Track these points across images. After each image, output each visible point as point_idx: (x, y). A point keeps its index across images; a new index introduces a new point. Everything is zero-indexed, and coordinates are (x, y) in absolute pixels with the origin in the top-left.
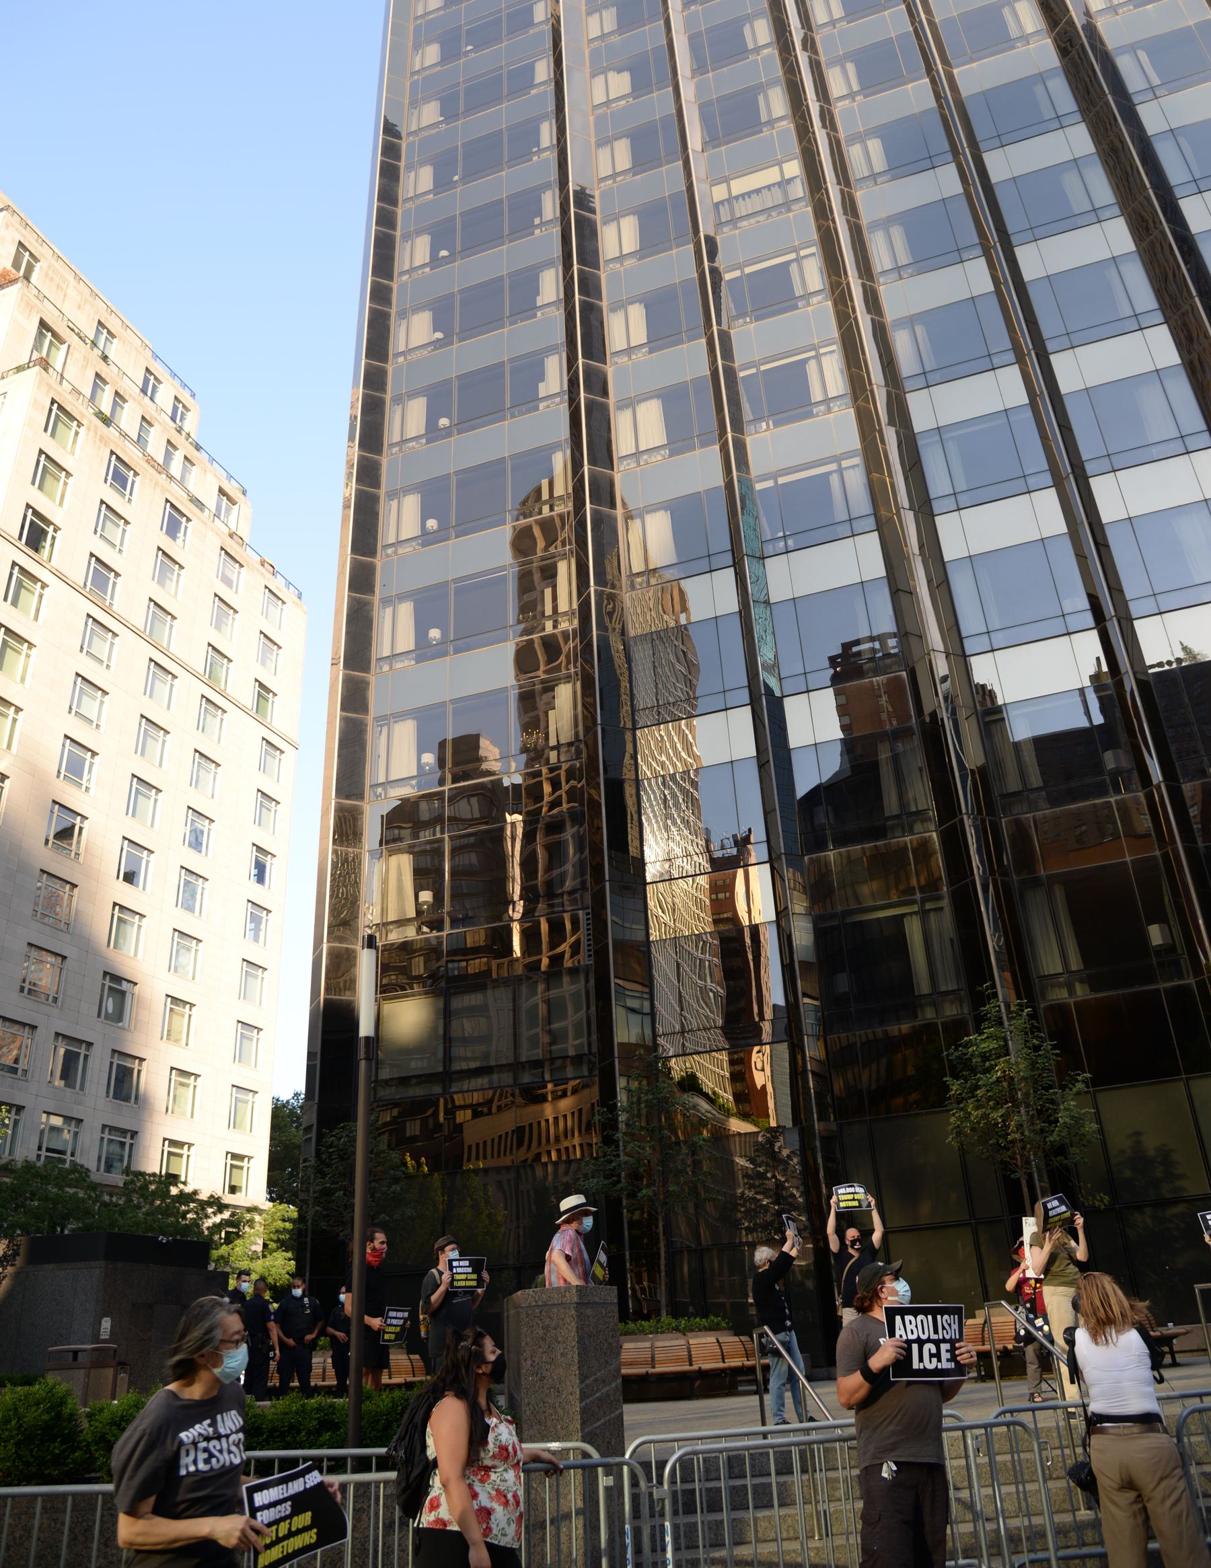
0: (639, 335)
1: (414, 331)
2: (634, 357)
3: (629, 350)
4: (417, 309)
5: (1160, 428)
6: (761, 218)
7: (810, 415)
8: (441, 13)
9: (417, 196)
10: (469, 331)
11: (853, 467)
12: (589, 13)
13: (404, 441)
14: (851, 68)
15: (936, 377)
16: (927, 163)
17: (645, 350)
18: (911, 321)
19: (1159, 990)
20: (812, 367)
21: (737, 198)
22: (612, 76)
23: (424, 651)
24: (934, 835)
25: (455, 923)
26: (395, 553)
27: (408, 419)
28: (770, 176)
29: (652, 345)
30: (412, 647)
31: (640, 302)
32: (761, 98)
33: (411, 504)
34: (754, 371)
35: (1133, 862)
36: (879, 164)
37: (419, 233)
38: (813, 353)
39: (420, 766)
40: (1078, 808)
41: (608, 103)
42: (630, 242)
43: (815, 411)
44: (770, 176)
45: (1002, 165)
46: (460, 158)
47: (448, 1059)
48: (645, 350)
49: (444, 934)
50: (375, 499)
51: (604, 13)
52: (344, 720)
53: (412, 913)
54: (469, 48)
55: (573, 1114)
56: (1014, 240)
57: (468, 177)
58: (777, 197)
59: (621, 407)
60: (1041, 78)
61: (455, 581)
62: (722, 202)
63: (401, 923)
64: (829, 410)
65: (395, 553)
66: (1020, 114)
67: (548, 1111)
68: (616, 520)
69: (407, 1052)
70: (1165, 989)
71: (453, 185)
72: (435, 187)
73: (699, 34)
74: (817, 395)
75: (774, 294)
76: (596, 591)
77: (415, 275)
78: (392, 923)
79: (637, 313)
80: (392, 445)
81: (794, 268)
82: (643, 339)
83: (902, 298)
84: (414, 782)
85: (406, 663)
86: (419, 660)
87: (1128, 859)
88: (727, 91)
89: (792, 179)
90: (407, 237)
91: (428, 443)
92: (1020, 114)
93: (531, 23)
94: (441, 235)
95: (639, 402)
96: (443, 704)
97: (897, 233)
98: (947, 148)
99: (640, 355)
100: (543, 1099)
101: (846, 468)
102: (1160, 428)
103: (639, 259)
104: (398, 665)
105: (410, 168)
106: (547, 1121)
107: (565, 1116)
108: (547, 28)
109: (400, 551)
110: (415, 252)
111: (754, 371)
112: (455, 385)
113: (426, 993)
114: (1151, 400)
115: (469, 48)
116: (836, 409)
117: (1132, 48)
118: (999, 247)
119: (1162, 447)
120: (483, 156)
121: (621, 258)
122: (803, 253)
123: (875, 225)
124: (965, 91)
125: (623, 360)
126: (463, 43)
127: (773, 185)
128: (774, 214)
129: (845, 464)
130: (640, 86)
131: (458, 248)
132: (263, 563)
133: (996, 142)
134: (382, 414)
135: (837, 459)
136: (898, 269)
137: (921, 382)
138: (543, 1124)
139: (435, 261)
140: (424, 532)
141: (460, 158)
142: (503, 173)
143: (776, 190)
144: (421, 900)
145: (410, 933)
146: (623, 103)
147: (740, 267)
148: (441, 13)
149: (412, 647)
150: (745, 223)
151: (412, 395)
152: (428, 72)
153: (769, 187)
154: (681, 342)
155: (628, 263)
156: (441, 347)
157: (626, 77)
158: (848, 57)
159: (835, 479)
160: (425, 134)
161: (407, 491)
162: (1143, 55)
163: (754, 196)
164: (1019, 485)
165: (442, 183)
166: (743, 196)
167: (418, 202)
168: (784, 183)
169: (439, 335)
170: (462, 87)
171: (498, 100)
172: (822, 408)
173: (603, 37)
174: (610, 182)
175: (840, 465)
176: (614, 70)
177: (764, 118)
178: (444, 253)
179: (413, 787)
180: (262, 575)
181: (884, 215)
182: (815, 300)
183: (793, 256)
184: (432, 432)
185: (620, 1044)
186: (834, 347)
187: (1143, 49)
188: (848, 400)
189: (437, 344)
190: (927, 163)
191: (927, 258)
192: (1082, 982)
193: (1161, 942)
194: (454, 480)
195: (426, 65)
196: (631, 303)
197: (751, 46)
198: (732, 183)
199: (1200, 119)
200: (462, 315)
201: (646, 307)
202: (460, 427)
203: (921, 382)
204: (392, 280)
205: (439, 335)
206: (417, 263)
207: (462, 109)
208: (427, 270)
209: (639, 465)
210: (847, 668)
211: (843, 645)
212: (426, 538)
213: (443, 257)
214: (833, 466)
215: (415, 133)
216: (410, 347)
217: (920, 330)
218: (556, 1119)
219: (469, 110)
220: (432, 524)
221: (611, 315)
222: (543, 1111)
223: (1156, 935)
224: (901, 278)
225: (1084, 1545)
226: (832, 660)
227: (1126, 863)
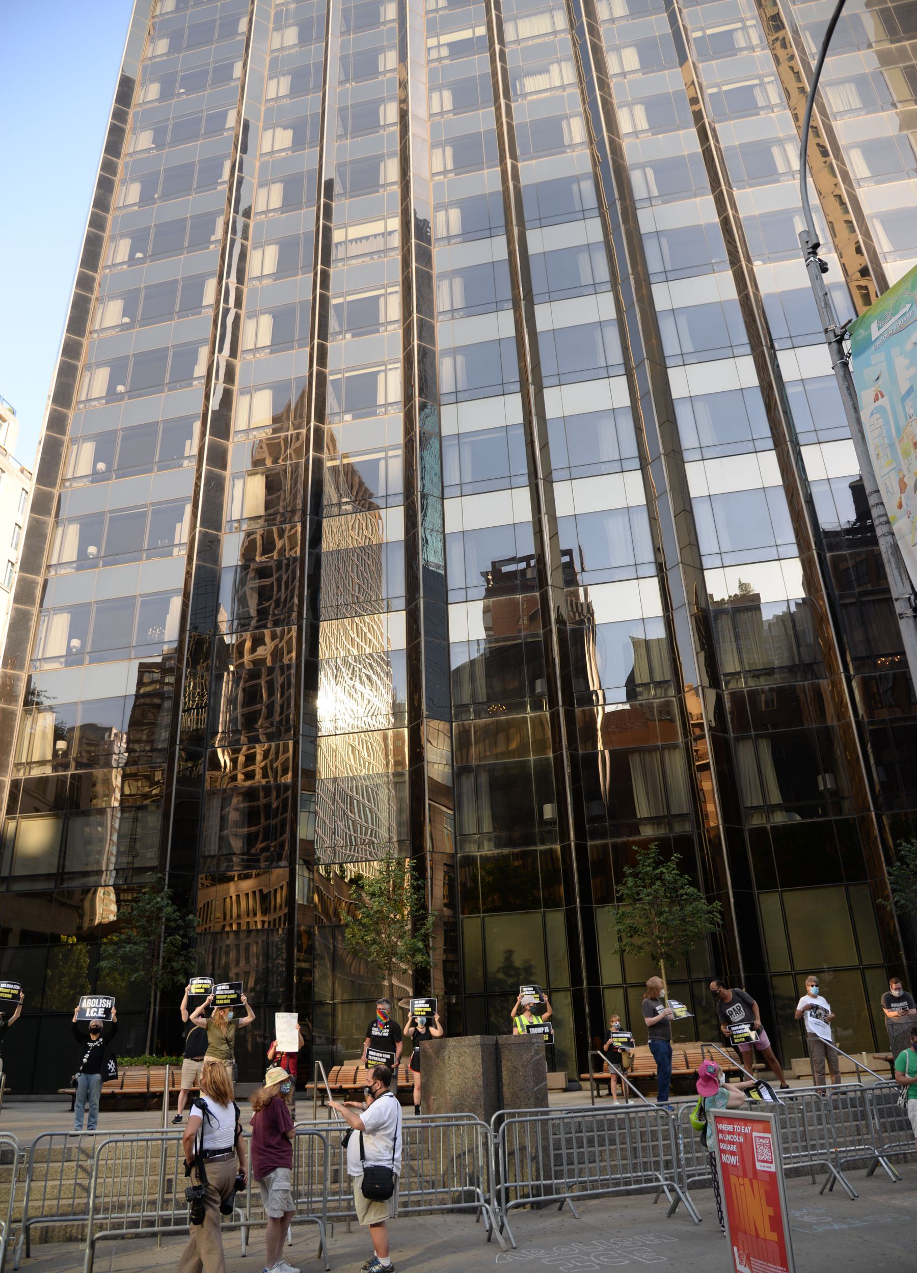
0: (265, 339)
1: (109, 314)
2: (258, 355)
3: (256, 350)
4: (112, 298)
5: (609, 452)
6: (367, 259)
7: (374, 414)
8: (165, 58)
9: (125, 206)
10: (148, 320)
11: (396, 456)
12: (271, 78)
13: (88, 400)
14: (449, 150)
15: (466, 395)
16: (487, 233)
17: (268, 351)
18: (454, 352)
19: (536, 850)
20: (381, 377)
21: (351, 241)
22: (279, 131)
23: (83, 562)
24: (406, 731)
25: (79, 765)
26: (71, 485)
27: (95, 383)
28: (377, 227)
29: (273, 348)
30: (75, 559)
31: (270, 313)
32: (382, 165)
33: (88, 449)
34: (339, 376)
35: (529, 761)
36: (456, 229)
37: (123, 236)
38: (383, 368)
39: (69, 648)
40: (507, 720)
41: (273, 152)
42: (270, 266)
43: (378, 411)
44: (377, 227)
45: (539, 241)
46: (161, 180)
47: (62, 864)
48: (268, 351)
49: (69, 773)
50: (60, 443)
51: (282, 79)
52: (16, 610)
53: (49, 757)
54: (182, 91)
55: (254, 892)
56: (536, 299)
57: (166, 196)
58: (379, 244)
59: (242, 393)
60: (577, 179)
61: (111, 512)
62: (340, 243)
63: (42, 763)
64: (386, 413)
65: (71, 485)
66: (558, 204)
67: (232, 889)
68: (224, 478)
69: (34, 860)
70: (541, 851)
71: (154, 201)
72: (140, 201)
73: (346, 108)
74: (381, 400)
75: (365, 318)
76: (200, 531)
77: (115, 270)
78: (35, 762)
79: (266, 322)
80: (79, 402)
81: (382, 300)
82: (268, 342)
83: (450, 334)
84: (63, 660)
85: (68, 570)
86: (78, 569)
87: (532, 758)
88: (358, 156)
89: (390, 233)
90: (113, 238)
91: (106, 403)
92: (558, 204)
93: (230, 78)
94: (139, 241)
95: (256, 390)
96: (89, 604)
97: (458, 283)
98: (503, 223)
99: (263, 354)
100: (231, 879)
101: (391, 457)
102: (609, 452)
103: (274, 280)
104: (63, 572)
105: (123, 182)
106: (231, 897)
107: (247, 895)
108: (239, 83)
109: (75, 485)
110: (117, 252)
111: (339, 376)
112: (131, 361)
113: (53, 815)
114: (606, 429)
115: (182, 91)
116: (392, 412)
117: (642, 166)
118: (524, 302)
119: (607, 465)
120: (178, 181)
121: (261, 277)
122: (389, 290)
123: (442, 276)
124: (524, 181)
125: (250, 357)
126: (177, 86)
127: (379, 235)
128: (376, 257)
129: (391, 453)
130: (298, 143)
131: (149, 253)
132: (22, 471)
133: (537, 223)
134: (74, 377)
135: (385, 449)
136: (453, 311)
137: (452, 398)
138: (228, 900)
139: (132, 261)
140: (95, 472)
141: (161, 180)
142: (191, 197)
143: (380, 238)
144: (57, 747)
145: (48, 771)
146: (283, 154)
147: (342, 295)
148: (165, 58)
149: (75, 559)
150: (354, 262)
151: (100, 365)
152: (148, 106)
153: (375, 236)
154: (292, 348)
155: (266, 282)
156: (127, 329)
157: (289, 133)
158: (448, 142)
159: (382, 464)
160: (138, 156)
161: (86, 439)
162: (650, 172)
163: (364, 241)
164: (505, 483)
165: (146, 198)
166: (356, 240)
167: (125, 211)
168: (386, 234)
169: (126, 320)
170: (171, 123)
171: (196, 137)
172: (383, 410)
173: (277, 98)
174: (442, 177)
175: (386, 455)
176: (281, 127)
177: (382, 182)
178: (139, 255)
179: (61, 663)
180: (21, 479)
181: (450, 269)
182: (390, 328)
183: (382, 292)
184: (111, 395)
185: (300, 840)
186: (399, 365)
187: (651, 167)
188: (401, 406)
189: (123, 327)
190: (487, 233)
191: (474, 306)
192: (489, 840)
193: (550, 816)
194: (121, 434)
195: (148, 99)
196: (262, 314)
197: (382, 123)
198: (388, 221)
199: (685, 225)
200: (150, 305)
201: (274, 317)
202: (171, 385)
203: (452, 398)
204: (96, 272)
205: (126, 320)
206: (118, 261)
207: (168, 140)
208: (125, 267)
209: (248, 439)
210: (500, 581)
211: (493, 564)
212: (96, 477)
213: (139, 258)
214: (382, 455)
215: (130, 155)
216: (103, 327)
217: (460, 359)
218: (238, 896)
219: (174, 142)
220: (101, 466)
221: (248, 321)
222: (229, 889)
223: (549, 811)
224: (453, 318)
225: (715, 1180)
226: (484, 574)
227: (535, 760)
